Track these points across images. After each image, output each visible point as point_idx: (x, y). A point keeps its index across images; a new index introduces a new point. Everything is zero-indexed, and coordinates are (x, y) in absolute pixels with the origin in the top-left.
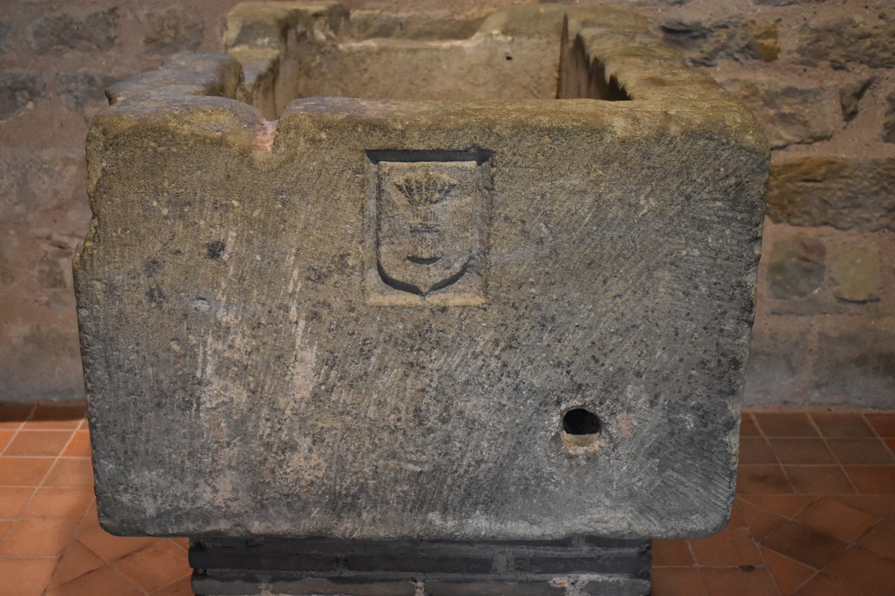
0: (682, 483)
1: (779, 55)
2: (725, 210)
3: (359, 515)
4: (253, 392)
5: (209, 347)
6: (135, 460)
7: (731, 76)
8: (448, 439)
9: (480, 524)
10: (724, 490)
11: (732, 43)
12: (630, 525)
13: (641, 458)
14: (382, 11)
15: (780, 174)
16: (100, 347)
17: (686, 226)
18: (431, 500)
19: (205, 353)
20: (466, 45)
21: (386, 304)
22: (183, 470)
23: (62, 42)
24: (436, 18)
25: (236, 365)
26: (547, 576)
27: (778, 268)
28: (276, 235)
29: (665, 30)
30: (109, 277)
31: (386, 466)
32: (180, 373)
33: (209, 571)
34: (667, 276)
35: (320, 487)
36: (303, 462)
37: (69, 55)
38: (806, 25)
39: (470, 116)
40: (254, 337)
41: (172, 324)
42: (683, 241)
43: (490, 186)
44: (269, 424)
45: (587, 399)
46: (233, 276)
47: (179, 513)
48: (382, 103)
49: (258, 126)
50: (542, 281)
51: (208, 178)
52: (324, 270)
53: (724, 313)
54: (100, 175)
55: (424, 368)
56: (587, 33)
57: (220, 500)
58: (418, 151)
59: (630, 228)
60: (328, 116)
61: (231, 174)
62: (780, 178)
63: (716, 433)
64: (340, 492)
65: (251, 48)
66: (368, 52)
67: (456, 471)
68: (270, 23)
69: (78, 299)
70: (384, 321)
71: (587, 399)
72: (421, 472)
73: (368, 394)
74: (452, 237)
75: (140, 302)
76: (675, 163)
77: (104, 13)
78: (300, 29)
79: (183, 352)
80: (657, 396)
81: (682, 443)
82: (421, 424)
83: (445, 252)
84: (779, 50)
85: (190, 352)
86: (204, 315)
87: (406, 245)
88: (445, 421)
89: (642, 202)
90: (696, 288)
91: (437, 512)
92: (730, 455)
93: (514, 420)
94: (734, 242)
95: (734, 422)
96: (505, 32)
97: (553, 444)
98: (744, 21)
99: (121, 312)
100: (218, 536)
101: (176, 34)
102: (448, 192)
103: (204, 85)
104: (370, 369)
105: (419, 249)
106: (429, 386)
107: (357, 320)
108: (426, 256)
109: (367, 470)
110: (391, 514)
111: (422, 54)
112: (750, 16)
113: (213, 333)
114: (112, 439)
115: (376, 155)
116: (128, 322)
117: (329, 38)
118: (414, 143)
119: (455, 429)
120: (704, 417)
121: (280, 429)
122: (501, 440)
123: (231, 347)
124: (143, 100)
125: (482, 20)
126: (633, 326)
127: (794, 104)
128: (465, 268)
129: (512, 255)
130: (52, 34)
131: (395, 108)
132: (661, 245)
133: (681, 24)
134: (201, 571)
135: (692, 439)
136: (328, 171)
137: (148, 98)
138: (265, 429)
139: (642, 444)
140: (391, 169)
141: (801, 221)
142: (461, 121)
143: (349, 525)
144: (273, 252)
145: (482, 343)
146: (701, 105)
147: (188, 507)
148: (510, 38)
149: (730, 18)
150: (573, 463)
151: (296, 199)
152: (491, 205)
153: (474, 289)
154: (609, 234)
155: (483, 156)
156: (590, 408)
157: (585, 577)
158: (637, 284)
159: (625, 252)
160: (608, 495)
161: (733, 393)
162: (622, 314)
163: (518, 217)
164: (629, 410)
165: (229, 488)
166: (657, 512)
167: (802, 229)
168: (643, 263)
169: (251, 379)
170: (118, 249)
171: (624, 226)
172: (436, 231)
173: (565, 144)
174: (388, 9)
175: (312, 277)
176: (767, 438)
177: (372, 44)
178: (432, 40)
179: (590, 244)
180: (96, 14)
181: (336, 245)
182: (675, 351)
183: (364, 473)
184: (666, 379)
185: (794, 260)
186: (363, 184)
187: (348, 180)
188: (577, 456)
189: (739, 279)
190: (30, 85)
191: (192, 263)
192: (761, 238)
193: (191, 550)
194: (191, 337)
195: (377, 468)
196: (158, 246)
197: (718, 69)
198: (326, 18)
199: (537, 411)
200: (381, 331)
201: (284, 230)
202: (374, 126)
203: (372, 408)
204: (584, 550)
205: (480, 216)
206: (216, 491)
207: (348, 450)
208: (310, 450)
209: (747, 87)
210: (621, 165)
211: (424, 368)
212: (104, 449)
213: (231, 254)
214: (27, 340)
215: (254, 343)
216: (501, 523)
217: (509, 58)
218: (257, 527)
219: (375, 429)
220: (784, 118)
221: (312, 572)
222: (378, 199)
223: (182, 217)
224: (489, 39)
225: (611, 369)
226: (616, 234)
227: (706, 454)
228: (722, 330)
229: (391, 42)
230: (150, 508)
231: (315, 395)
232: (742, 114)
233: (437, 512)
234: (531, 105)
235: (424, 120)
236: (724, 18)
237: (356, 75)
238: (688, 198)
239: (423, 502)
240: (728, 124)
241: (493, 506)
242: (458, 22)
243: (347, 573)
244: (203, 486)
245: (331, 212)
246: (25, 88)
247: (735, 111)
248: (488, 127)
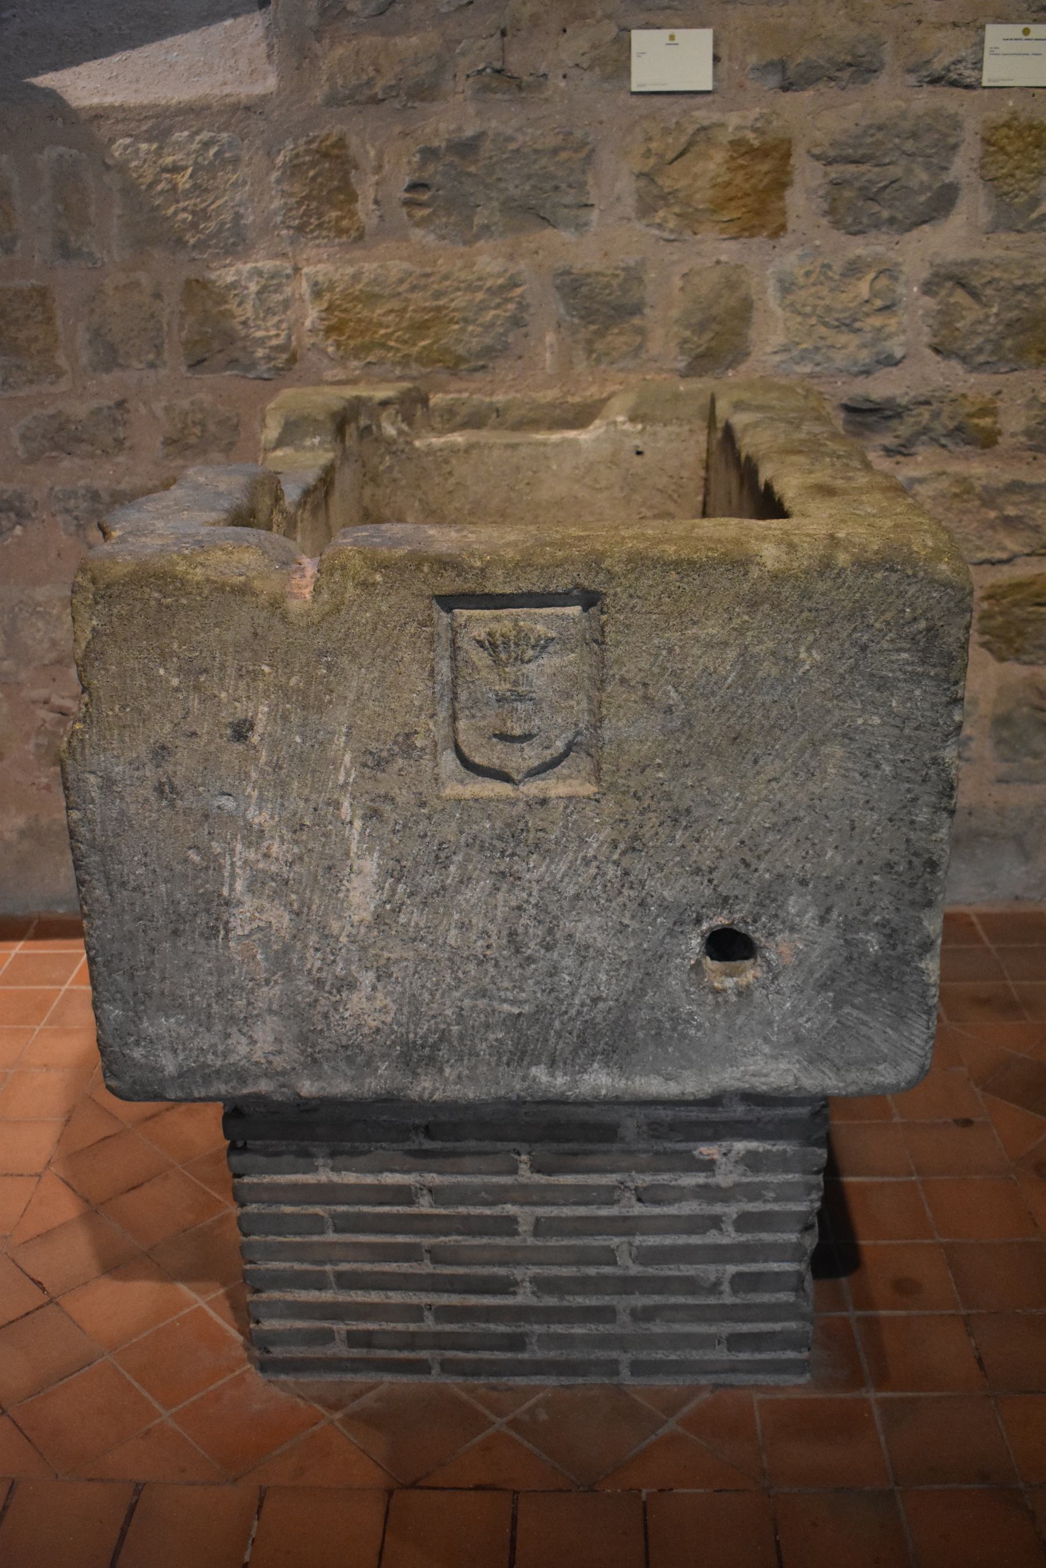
0: (864, 1023)
1: (1000, 439)
2: (913, 663)
3: (441, 1071)
4: (298, 914)
5: (238, 856)
6: (148, 1003)
7: (937, 468)
8: (554, 971)
9: (599, 1080)
10: (919, 1034)
11: (936, 425)
12: (796, 1079)
13: (809, 992)
14: (472, 394)
15: (1004, 597)
16: (97, 859)
17: (862, 686)
18: (534, 1050)
19: (233, 864)
20: (583, 436)
21: (467, 797)
22: (209, 1016)
23: (57, 447)
24: (543, 401)
25: (273, 880)
26: (691, 1145)
27: (1003, 721)
28: (320, 709)
29: (848, 409)
30: (106, 768)
31: (473, 1008)
32: (201, 891)
33: (251, 1144)
34: (839, 752)
35: (388, 1036)
36: (365, 1004)
37: (66, 463)
38: (1035, 398)
39: (571, 546)
40: (296, 842)
41: (189, 827)
42: (859, 706)
43: (600, 639)
44: (319, 955)
45: (737, 916)
46: (266, 764)
47: (207, 1071)
48: (457, 531)
49: (295, 566)
50: (672, 762)
51: (229, 636)
52: (385, 754)
53: (915, 800)
54: (90, 636)
55: (519, 878)
56: (739, 420)
57: (259, 1053)
58: (503, 595)
59: (787, 690)
60: (384, 552)
61: (259, 630)
62: (1004, 601)
63: (909, 957)
64: (414, 1042)
65: (296, 450)
66: (454, 449)
67: (566, 1012)
68: (321, 418)
69: (67, 797)
70: (465, 818)
71: (737, 916)
72: (520, 1014)
73: (448, 914)
74: (551, 707)
75: (147, 800)
76: (845, 603)
77: (109, 408)
78: (363, 422)
79: (205, 864)
80: (829, 910)
81: (864, 970)
82: (518, 951)
83: (542, 727)
84: (999, 433)
85: (212, 864)
86: (231, 816)
87: (490, 718)
88: (548, 948)
89: (803, 655)
90: (877, 767)
91: (543, 1066)
92: (928, 985)
93: (641, 944)
94: (926, 705)
95: (932, 943)
96: (632, 419)
97: (693, 975)
98: (952, 395)
99: (122, 813)
100: (259, 1099)
101: (202, 431)
102: (544, 647)
103: (227, 511)
104: (449, 881)
105: (509, 724)
106: (527, 902)
107: (429, 818)
108: (518, 732)
109: (448, 1012)
110: (483, 1069)
111: (524, 451)
112: (960, 388)
113: (243, 838)
114: (118, 977)
115: (449, 602)
116: (131, 826)
117: (401, 432)
118: (498, 585)
119: (563, 958)
120: (891, 934)
121: (334, 961)
122: (623, 971)
123: (266, 856)
124: (145, 536)
125: (604, 401)
126: (795, 819)
127: (1022, 502)
128: (569, 748)
129: (631, 729)
130: (43, 437)
131: (472, 537)
132: (829, 711)
133: (868, 400)
134: (240, 1144)
135: (876, 965)
136: (385, 625)
137: (152, 532)
138: (314, 961)
139: (811, 972)
140: (469, 619)
141: (1033, 657)
142: (560, 554)
143: (427, 1084)
144: (318, 731)
145: (595, 845)
146: (879, 522)
147: (219, 1063)
148: (640, 427)
149: (934, 391)
150: (720, 999)
151: (344, 661)
152: (602, 664)
153: (584, 774)
154: (759, 699)
155: (589, 599)
156: (741, 928)
157: (740, 1146)
158: (799, 763)
159: (782, 722)
160: (766, 1040)
161: (930, 904)
162: (780, 804)
163: (638, 679)
164: (792, 929)
165: (271, 1039)
166: (832, 1061)
167: (1035, 669)
168: (805, 736)
169: (294, 897)
170: (116, 732)
171: (780, 688)
172: (531, 700)
173: (697, 582)
174: (480, 390)
175: (369, 763)
176: (992, 947)
177: (458, 438)
178: (537, 431)
179: (734, 712)
180: (100, 410)
181: (400, 720)
182: (852, 851)
183: (446, 1016)
184: (840, 887)
185: (1025, 710)
186: (431, 641)
187: (413, 635)
188: (725, 990)
189: (934, 754)
190: (17, 504)
191: (212, 748)
192: (962, 699)
193: (226, 1117)
194: (214, 844)
195: (462, 1009)
196: (168, 727)
197: (920, 458)
198: (397, 406)
199: (671, 933)
200: (461, 832)
201: (330, 702)
202: (445, 563)
203: (453, 932)
204: (739, 1111)
205: (589, 678)
206: (253, 1042)
207: (423, 987)
208: (374, 988)
209: (957, 481)
210: (773, 606)
211: (519, 878)
212: (107, 990)
213: (262, 735)
214: (23, 834)
215: (296, 850)
216: (627, 1079)
217: (639, 453)
218: (308, 1088)
219: (457, 959)
220: (1009, 523)
221: (384, 1145)
222: (453, 658)
223: (197, 688)
224: (612, 428)
225: (767, 876)
226: (768, 699)
227: (895, 985)
228: (912, 822)
229: (483, 435)
230: (170, 1065)
231: (378, 917)
232: (934, 535)
233: (543, 1066)
234: (653, 528)
235: (510, 554)
236: (925, 392)
237: (437, 480)
238: (864, 648)
239: (524, 1053)
240: (915, 549)
241: (616, 1057)
242: (573, 405)
243: (428, 1145)
244: (236, 1036)
245: (391, 678)
246: (12, 508)
247: (926, 531)
248: (594, 562)
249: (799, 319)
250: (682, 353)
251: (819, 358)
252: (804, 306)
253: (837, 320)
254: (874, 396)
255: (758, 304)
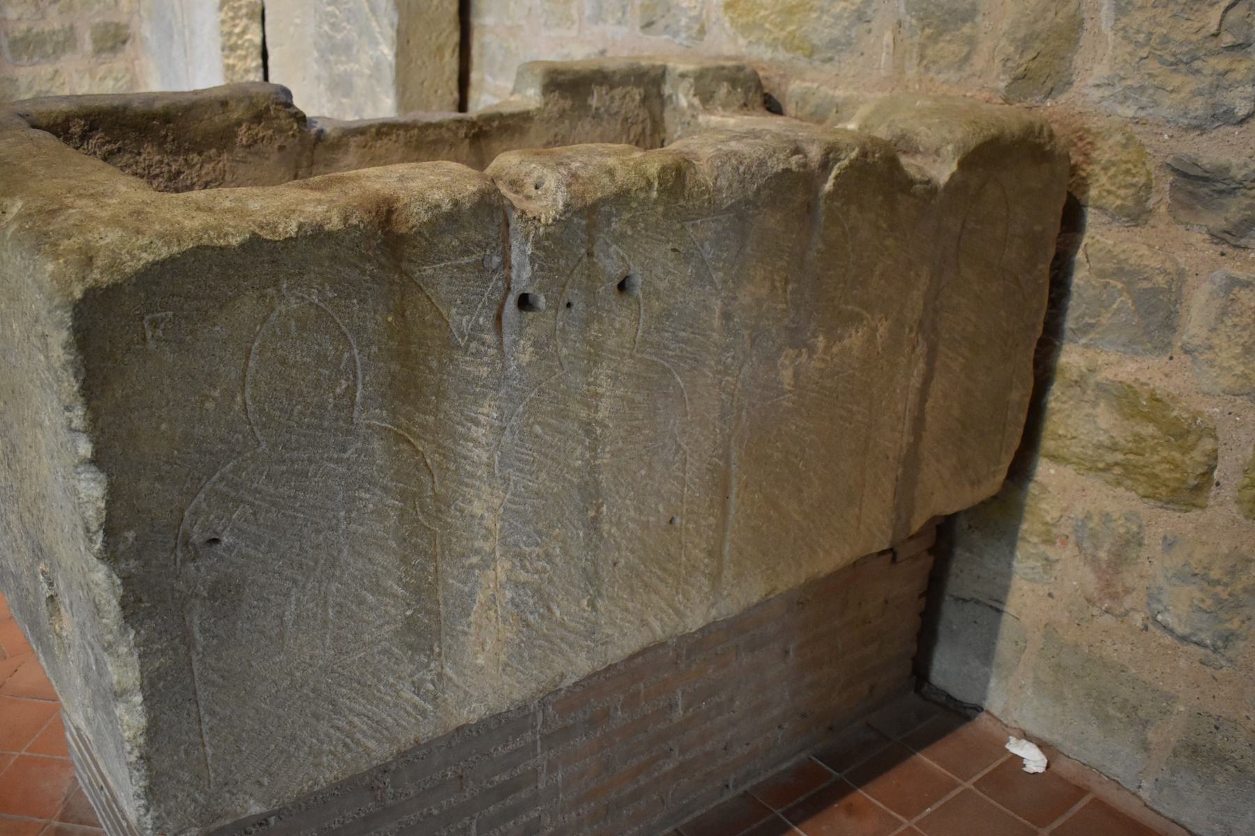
117: (691, 106)
249: (1130, 48)
250: (1004, 72)
251: (1144, 100)
252: (1138, 32)
253: (1174, 55)
254: (1204, 161)
255: (1088, 25)
